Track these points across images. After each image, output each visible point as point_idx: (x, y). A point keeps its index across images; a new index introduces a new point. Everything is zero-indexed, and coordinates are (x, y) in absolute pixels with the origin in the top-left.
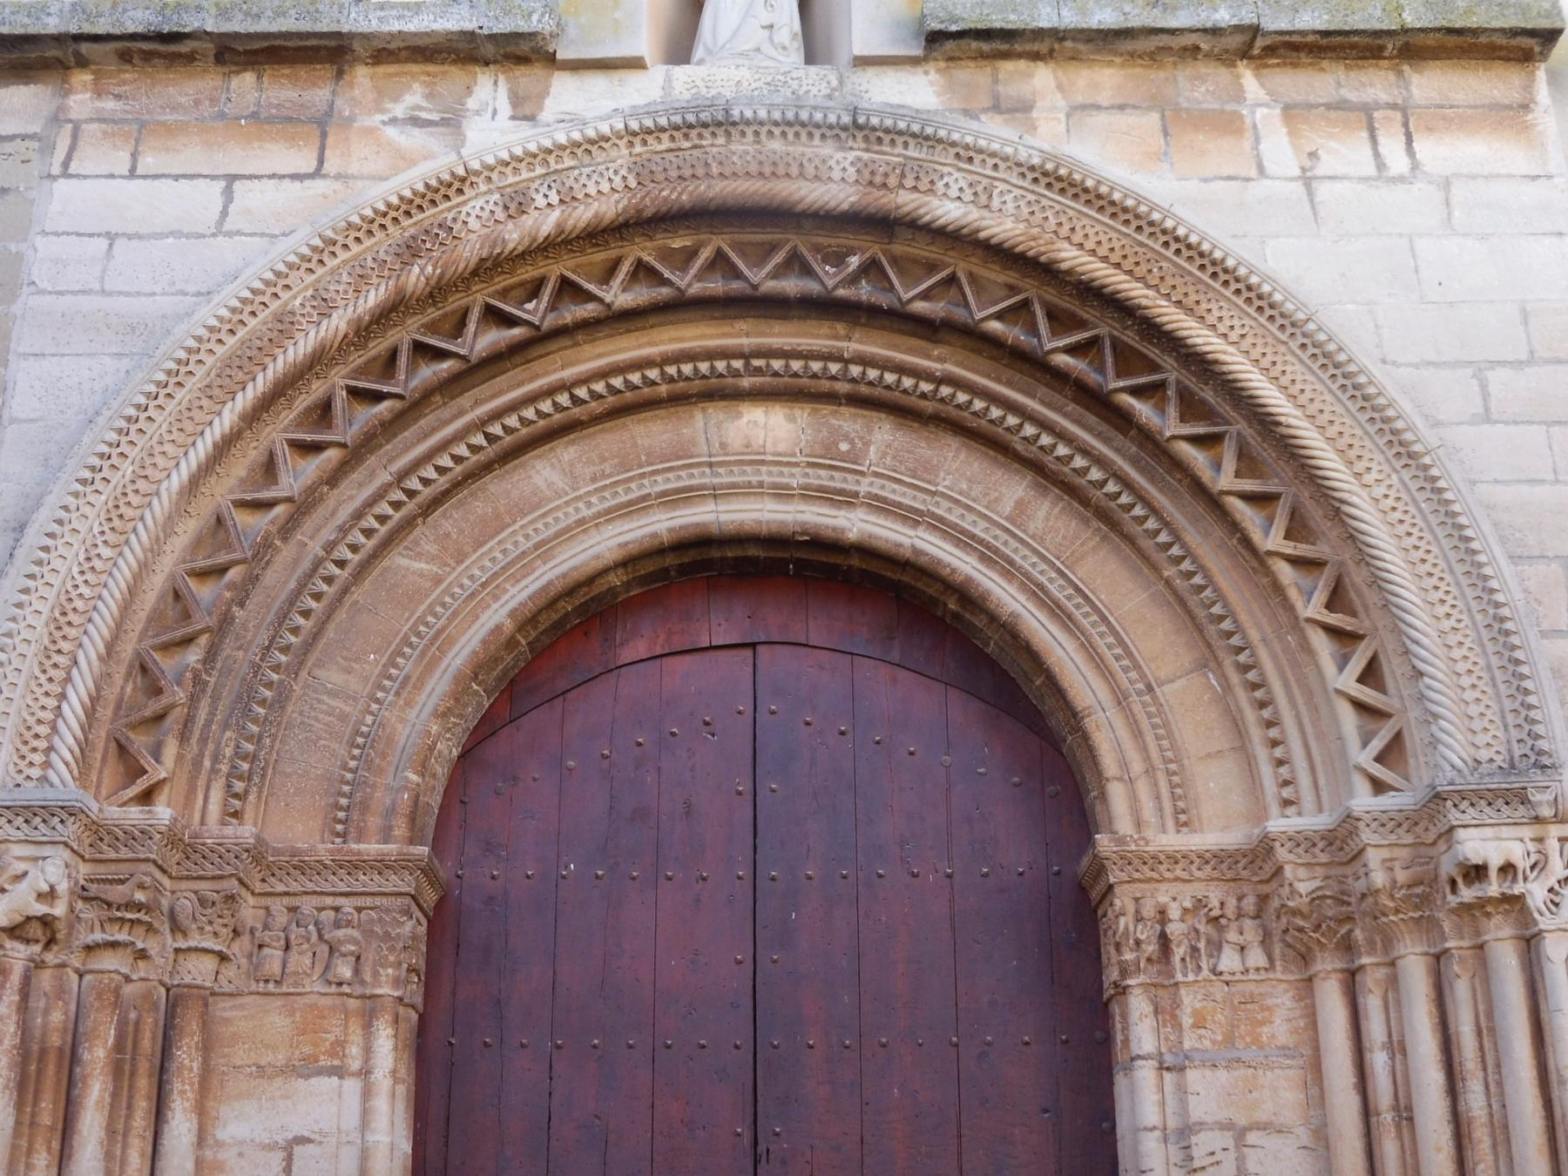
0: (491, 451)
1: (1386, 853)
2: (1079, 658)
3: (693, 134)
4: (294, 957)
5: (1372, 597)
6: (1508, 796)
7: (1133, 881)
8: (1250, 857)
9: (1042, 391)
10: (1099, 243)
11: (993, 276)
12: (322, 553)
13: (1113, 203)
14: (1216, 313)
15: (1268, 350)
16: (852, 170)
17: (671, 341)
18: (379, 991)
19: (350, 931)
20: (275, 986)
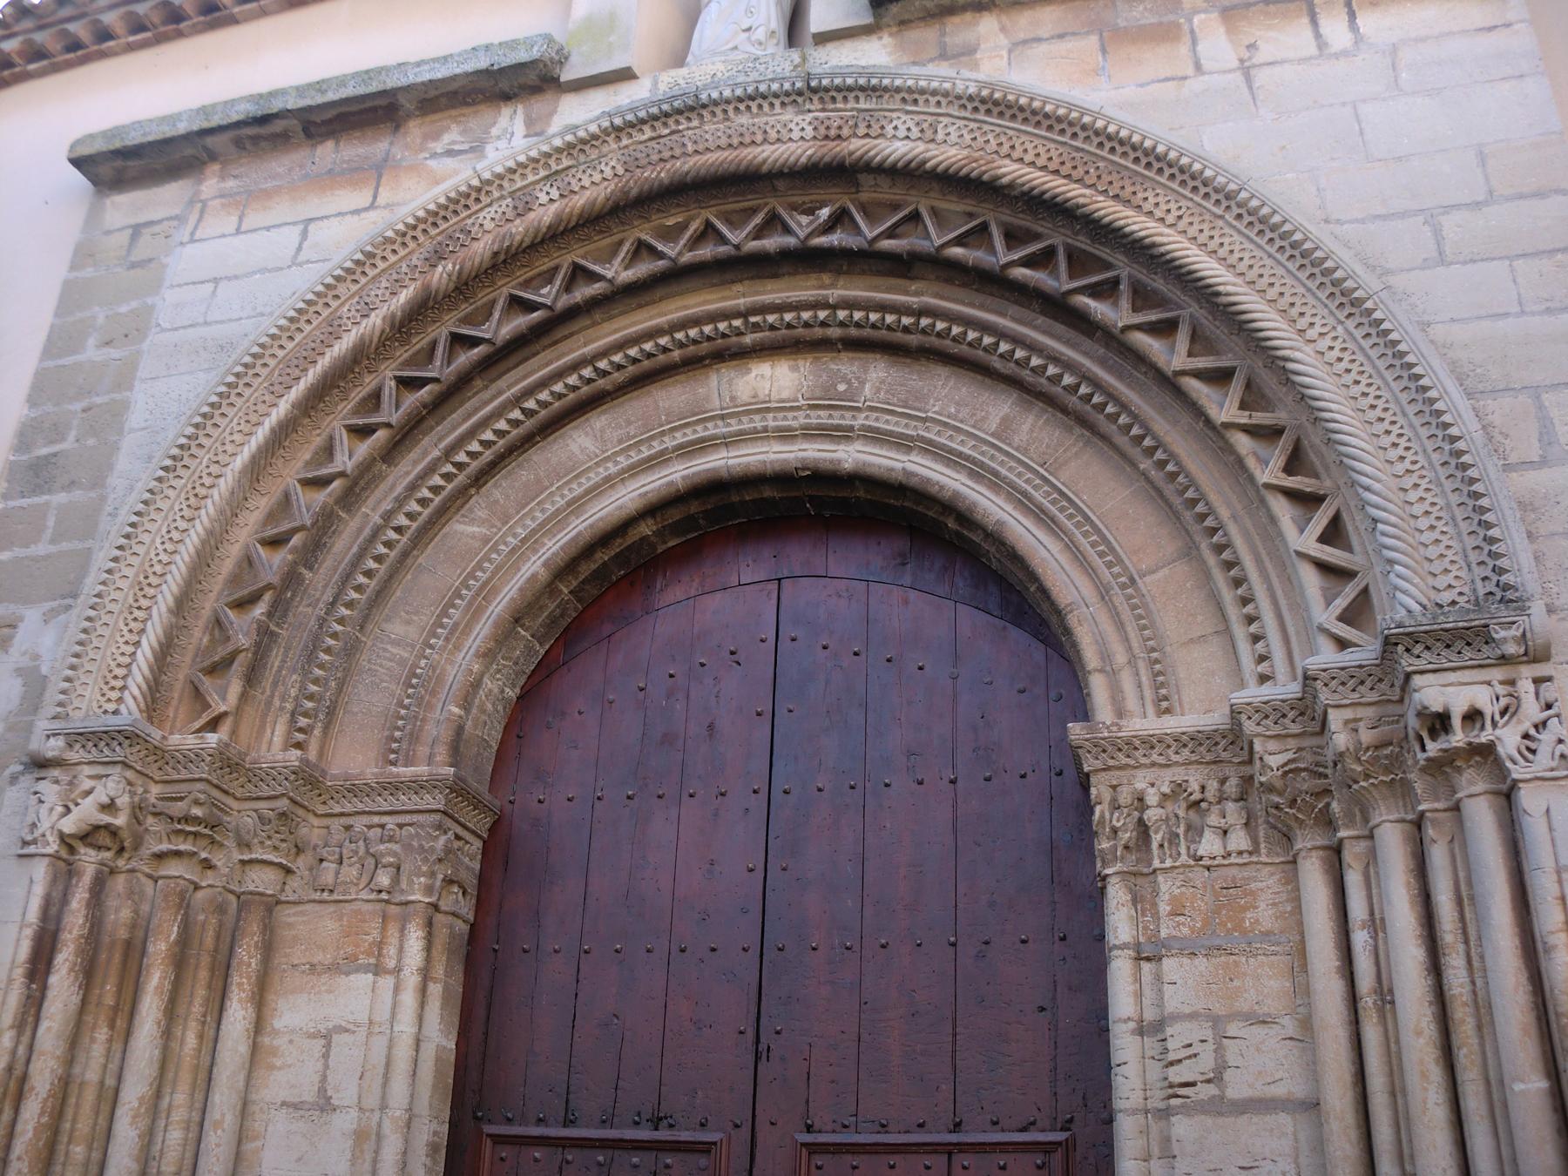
0: (530, 424)
1: (1348, 714)
2: (1064, 559)
3: (671, 121)
4: (345, 869)
5: (1331, 457)
6: (1464, 639)
7: (1108, 769)
8: (1231, 738)
9: (1013, 309)
10: (1038, 155)
11: (953, 207)
12: (380, 521)
13: (1047, 116)
14: (1152, 200)
15: (1205, 226)
16: (809, 129)
17: (677, 310)
18: (412, 898)
19: (389, 845)
20: (327, 894)
